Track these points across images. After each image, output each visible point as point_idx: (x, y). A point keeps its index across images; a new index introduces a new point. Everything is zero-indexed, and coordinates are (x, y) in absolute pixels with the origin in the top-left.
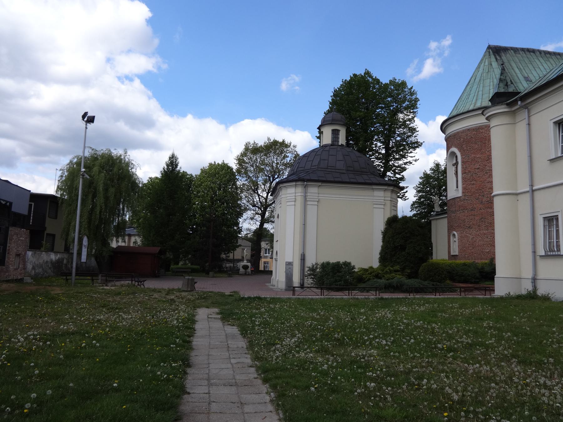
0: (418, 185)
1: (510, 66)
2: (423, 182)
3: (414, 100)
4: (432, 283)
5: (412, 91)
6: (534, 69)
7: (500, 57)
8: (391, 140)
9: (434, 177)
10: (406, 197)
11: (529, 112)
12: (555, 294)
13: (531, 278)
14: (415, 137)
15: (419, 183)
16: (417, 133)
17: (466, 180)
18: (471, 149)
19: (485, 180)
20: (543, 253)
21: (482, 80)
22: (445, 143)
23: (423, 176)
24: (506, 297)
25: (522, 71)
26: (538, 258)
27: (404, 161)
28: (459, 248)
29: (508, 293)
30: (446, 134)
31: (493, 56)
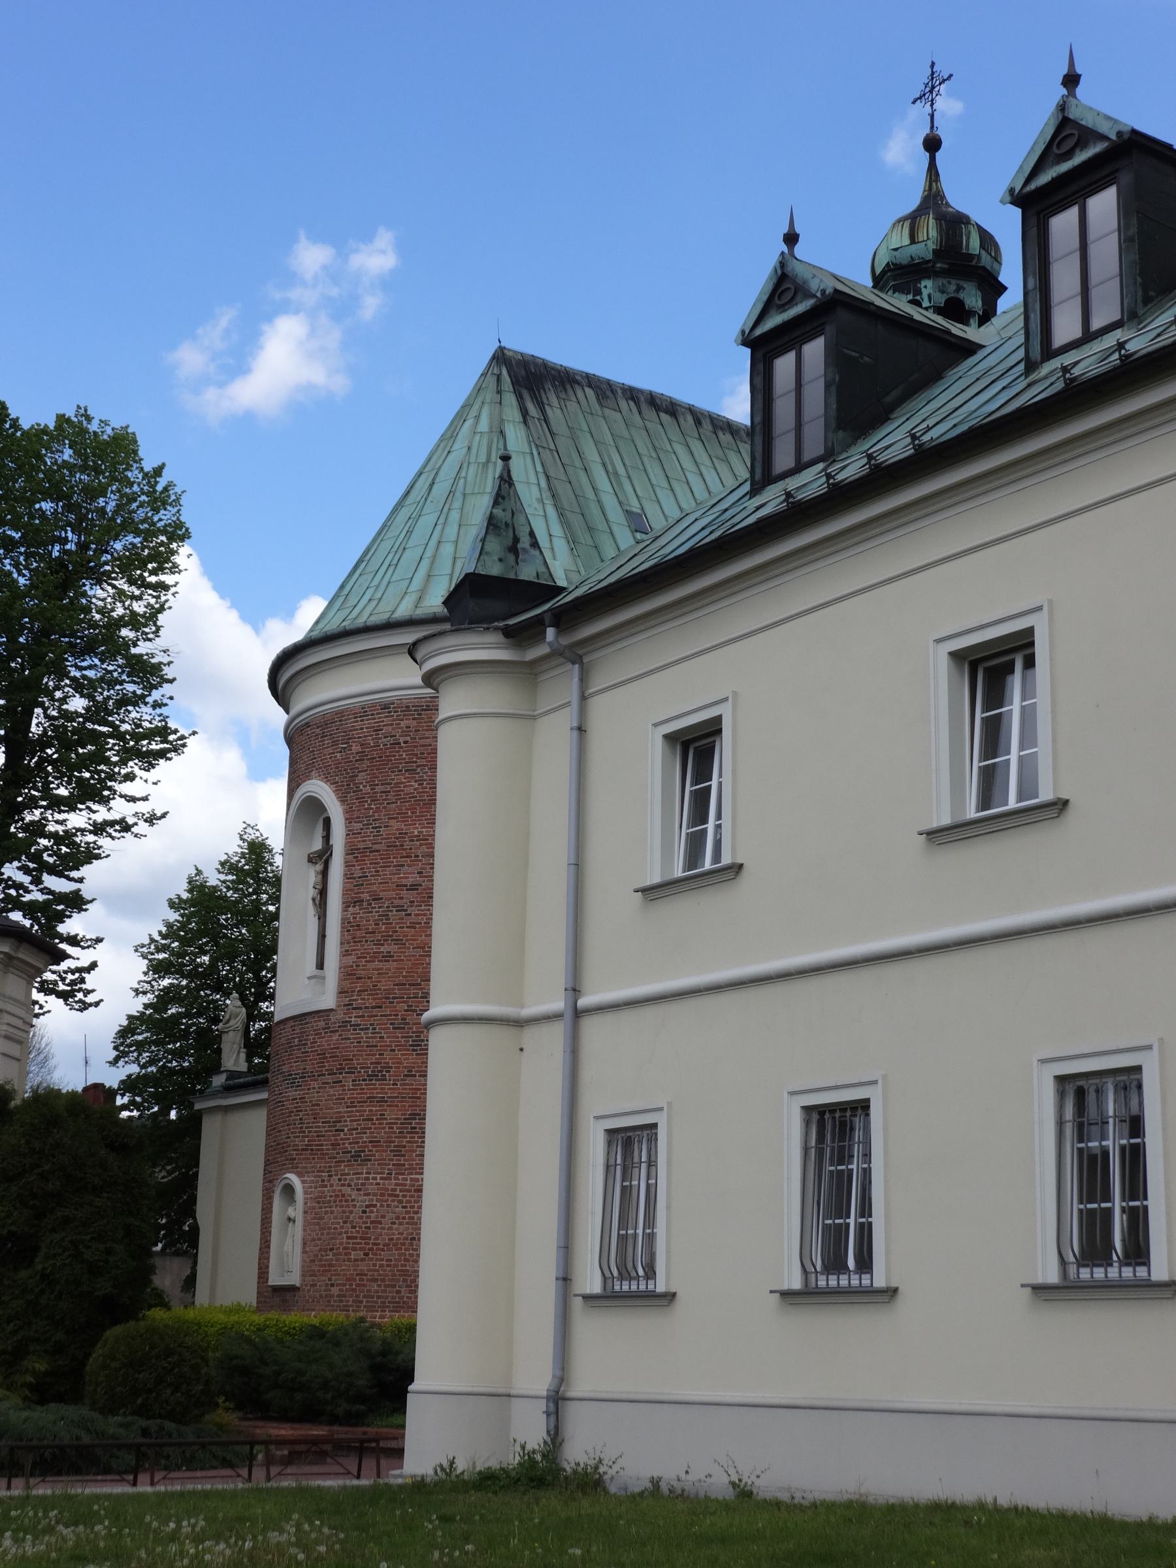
0: (157, 938)
1: (575, 456)
2: (183, 926)
3: (163, 532)
4: (143, 1423)
5: (159, 488)
6: (665, 484)
7: (541, 406)
8: (42, 705)
9: (237, 902)
10: (87, 992)
11: (584, 681)
12: (620, 1463)
13: (545, 1393)
14: (157, 705)
15: (164, 930)
16: (167, 689)
18: (391, 796)
20: (596, 1287)
21: (459, 495)
22: (283, 752)
23: (185, 896)
24: (438, 1484)
25: (620, 484)
26: (578, 1302)
27: (93, 816)
28: (304, 1252)
29: (445, 1464)
30: (293, 712)
31: (510, 399)
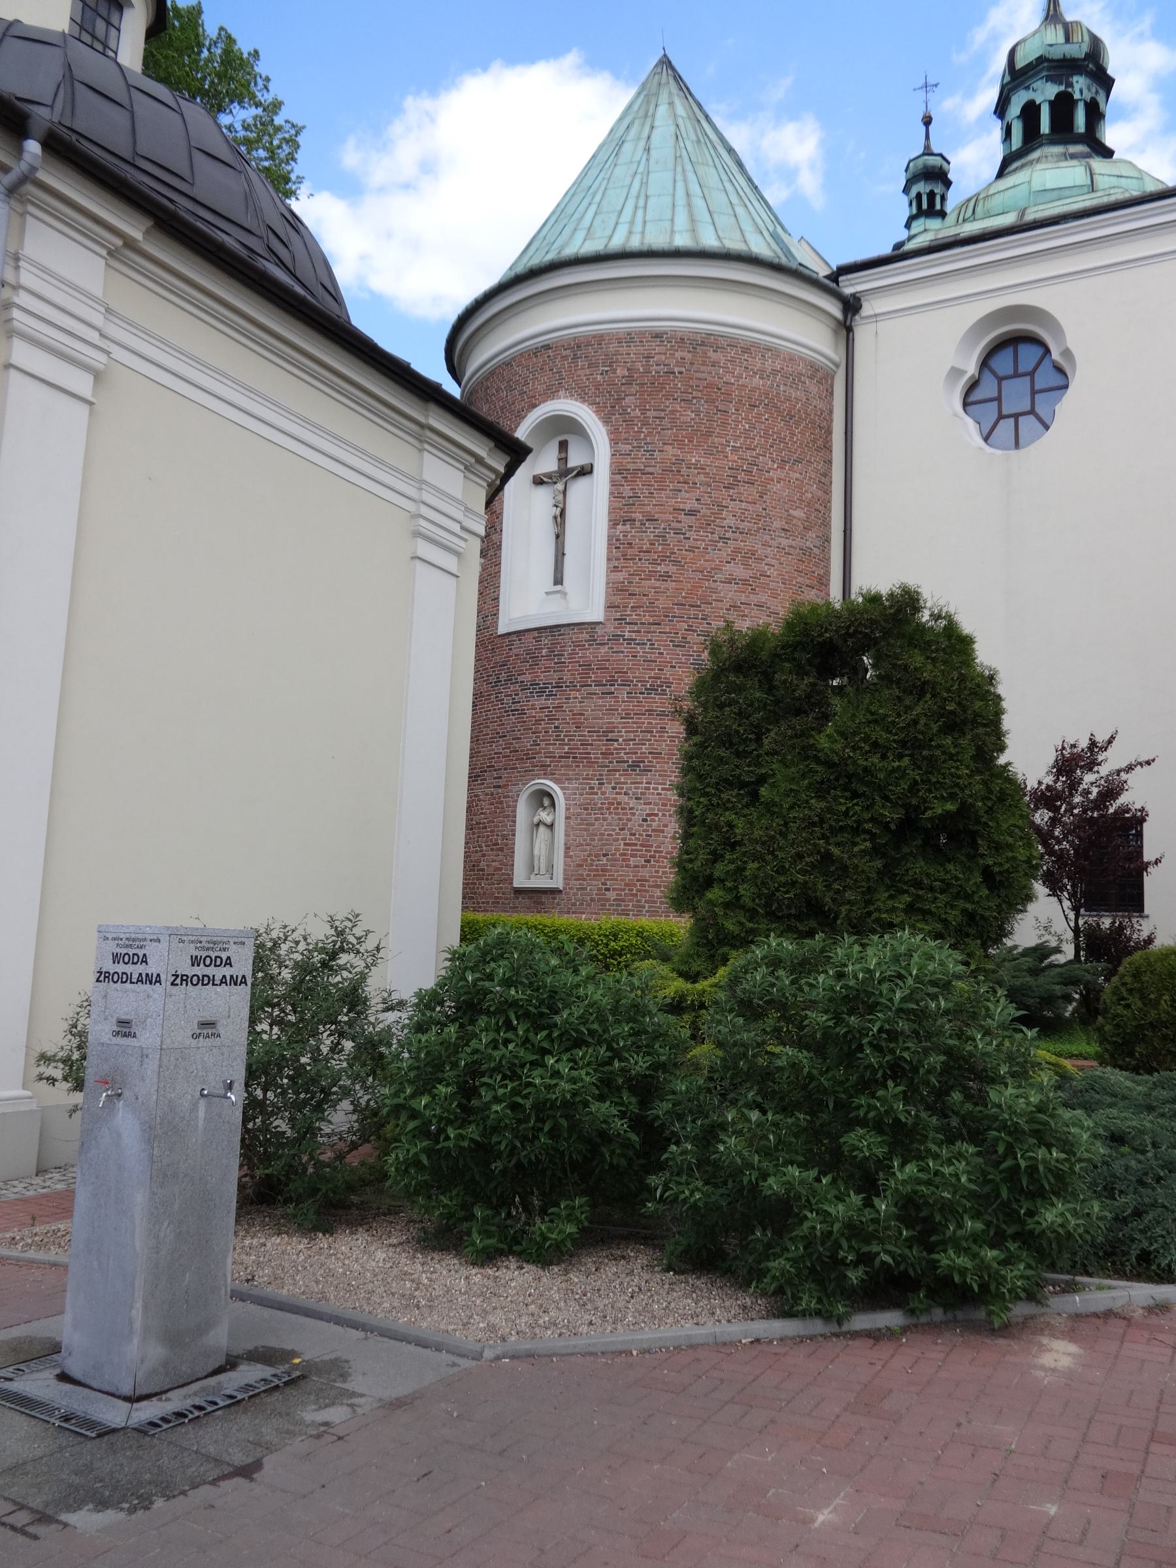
17: (629, 551)
18: (666, 422)
19: (718, 569)
28: (567, 856)
